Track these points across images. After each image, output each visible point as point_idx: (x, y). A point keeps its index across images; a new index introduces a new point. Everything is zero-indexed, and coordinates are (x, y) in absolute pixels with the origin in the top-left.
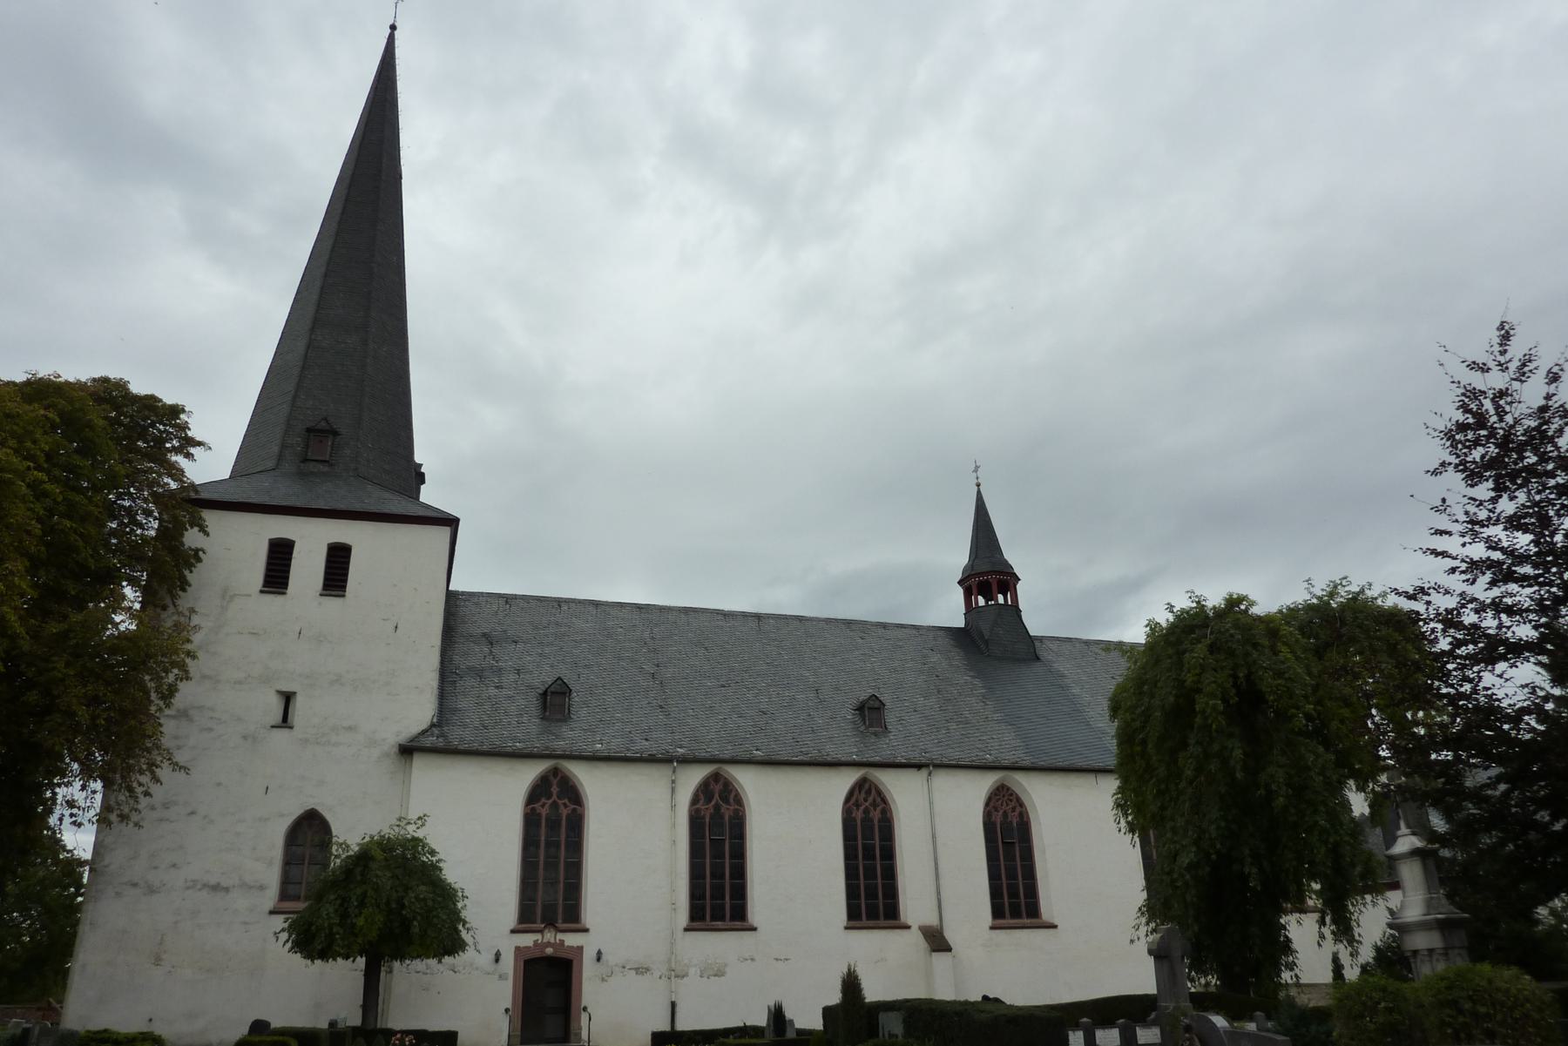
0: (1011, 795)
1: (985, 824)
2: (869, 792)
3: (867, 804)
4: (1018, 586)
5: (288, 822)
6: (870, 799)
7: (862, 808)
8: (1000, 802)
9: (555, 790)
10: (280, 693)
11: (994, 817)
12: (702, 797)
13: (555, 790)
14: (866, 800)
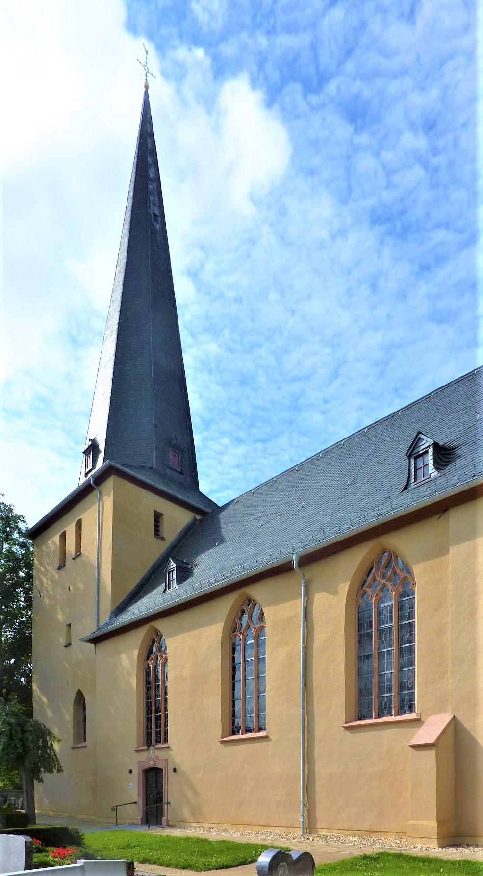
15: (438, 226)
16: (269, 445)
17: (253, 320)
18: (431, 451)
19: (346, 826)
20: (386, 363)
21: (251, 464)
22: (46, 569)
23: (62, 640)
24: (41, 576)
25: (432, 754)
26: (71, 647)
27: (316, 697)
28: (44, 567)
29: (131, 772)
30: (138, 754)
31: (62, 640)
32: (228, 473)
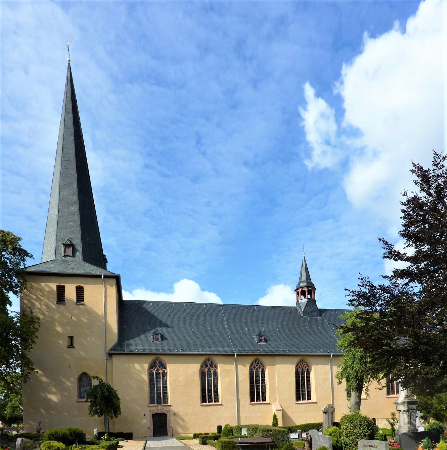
0: (305, 363)
1: (296, 372)
2: (258, 363)
3: (257, 367)
4: (315, 292)
5: (77, 377)
6: (258, 365)
7: (255, 368)
8: (301, 365)
9: (158, 364)
10: (166, 339)
11: (304, 370)
12: (204, 366)
13: (158, 364)
14: (257, 366)
22: (38, 298)
24: (32, 300)
27: (240, 395)
29: (144, 415)
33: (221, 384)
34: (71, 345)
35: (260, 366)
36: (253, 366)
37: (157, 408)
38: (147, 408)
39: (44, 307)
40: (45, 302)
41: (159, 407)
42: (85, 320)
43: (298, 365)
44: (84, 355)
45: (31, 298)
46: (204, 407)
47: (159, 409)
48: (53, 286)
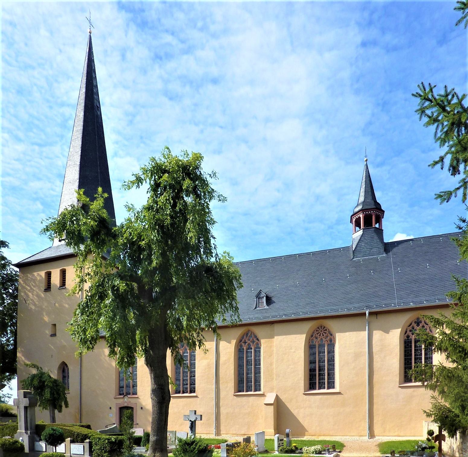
15: (167, 31)
16: (44, 149)
17: (26, 45)
18: (265, 298)
19: (234, 432)
20: (134, 116)
21: (30, 161)
22: (31, 288)
23: (47, 332)
24: (27, 291)
25: (272, 407)
26: (56, 337)
27: (221, 382)
28: (29, 286)
29: (110, 408)
30: (115, 399)
31: (48, 332)
32: (9, 163)
33: (340, 361)
34: (54, 335)
35: (253, 339)
36: (243, 340)
37: (123, 400)
38: (114, 400)
39: (35, 297)
40: (37, 293)
41: (126, 399)
42: (67, 306)
43: (243, 337)
44: (66, 344)
45: (26, 289)
46: (239, 399)
47: (126, 401)
48: (43, 274)
